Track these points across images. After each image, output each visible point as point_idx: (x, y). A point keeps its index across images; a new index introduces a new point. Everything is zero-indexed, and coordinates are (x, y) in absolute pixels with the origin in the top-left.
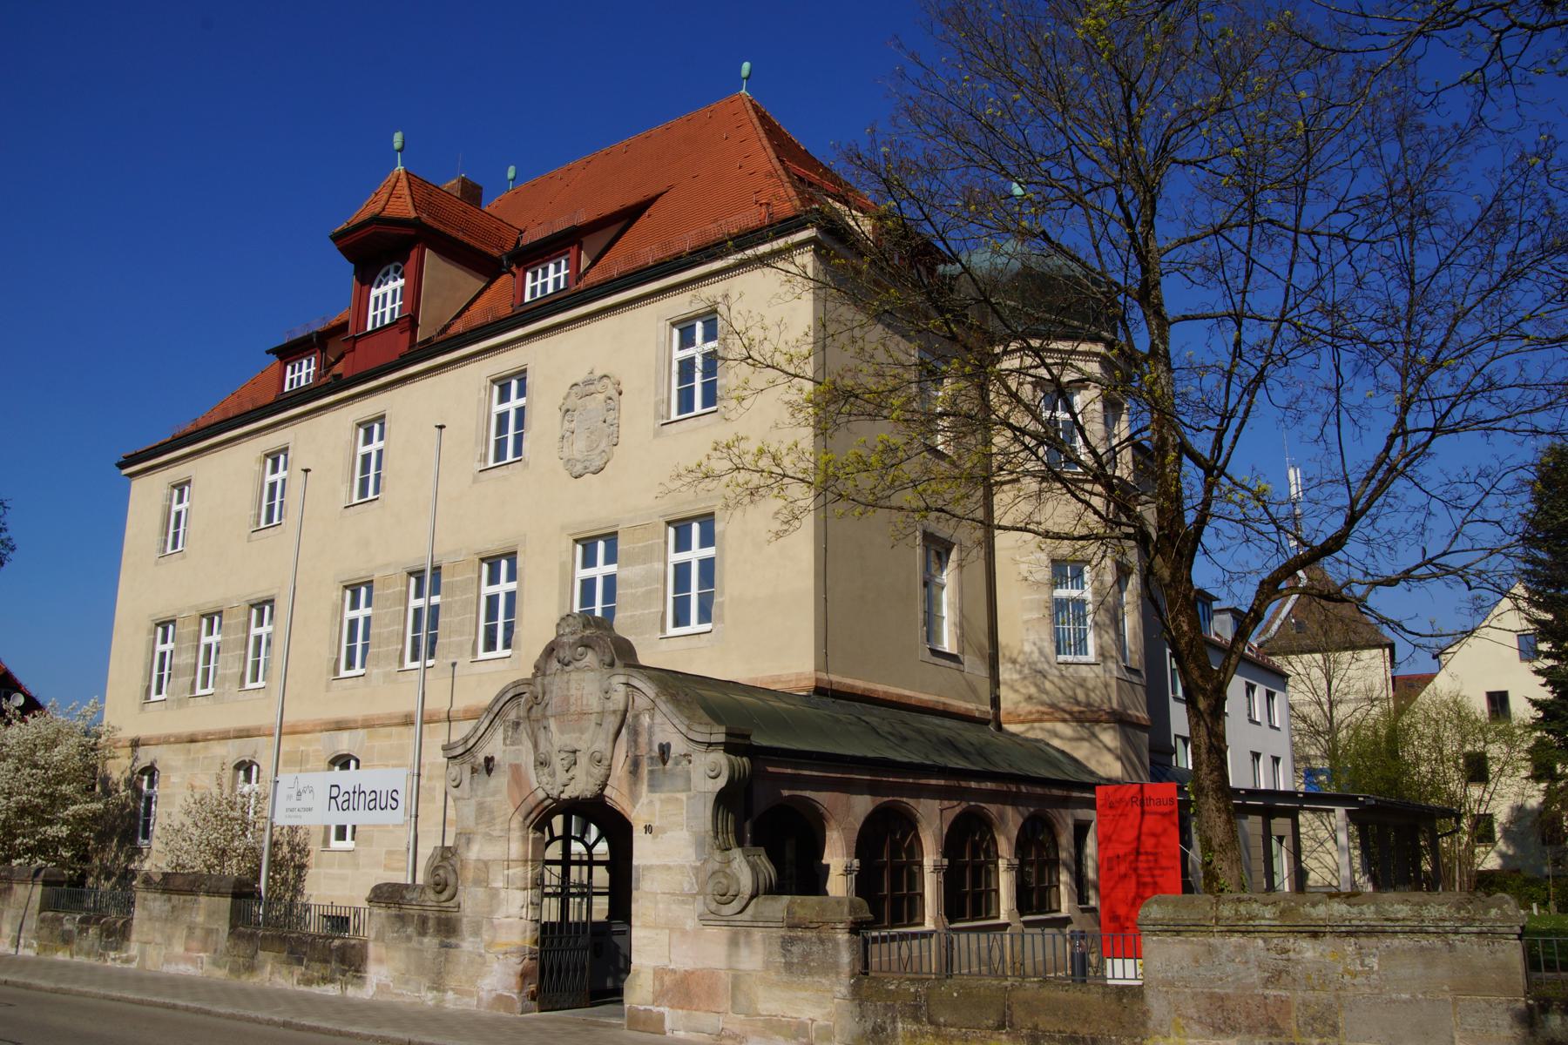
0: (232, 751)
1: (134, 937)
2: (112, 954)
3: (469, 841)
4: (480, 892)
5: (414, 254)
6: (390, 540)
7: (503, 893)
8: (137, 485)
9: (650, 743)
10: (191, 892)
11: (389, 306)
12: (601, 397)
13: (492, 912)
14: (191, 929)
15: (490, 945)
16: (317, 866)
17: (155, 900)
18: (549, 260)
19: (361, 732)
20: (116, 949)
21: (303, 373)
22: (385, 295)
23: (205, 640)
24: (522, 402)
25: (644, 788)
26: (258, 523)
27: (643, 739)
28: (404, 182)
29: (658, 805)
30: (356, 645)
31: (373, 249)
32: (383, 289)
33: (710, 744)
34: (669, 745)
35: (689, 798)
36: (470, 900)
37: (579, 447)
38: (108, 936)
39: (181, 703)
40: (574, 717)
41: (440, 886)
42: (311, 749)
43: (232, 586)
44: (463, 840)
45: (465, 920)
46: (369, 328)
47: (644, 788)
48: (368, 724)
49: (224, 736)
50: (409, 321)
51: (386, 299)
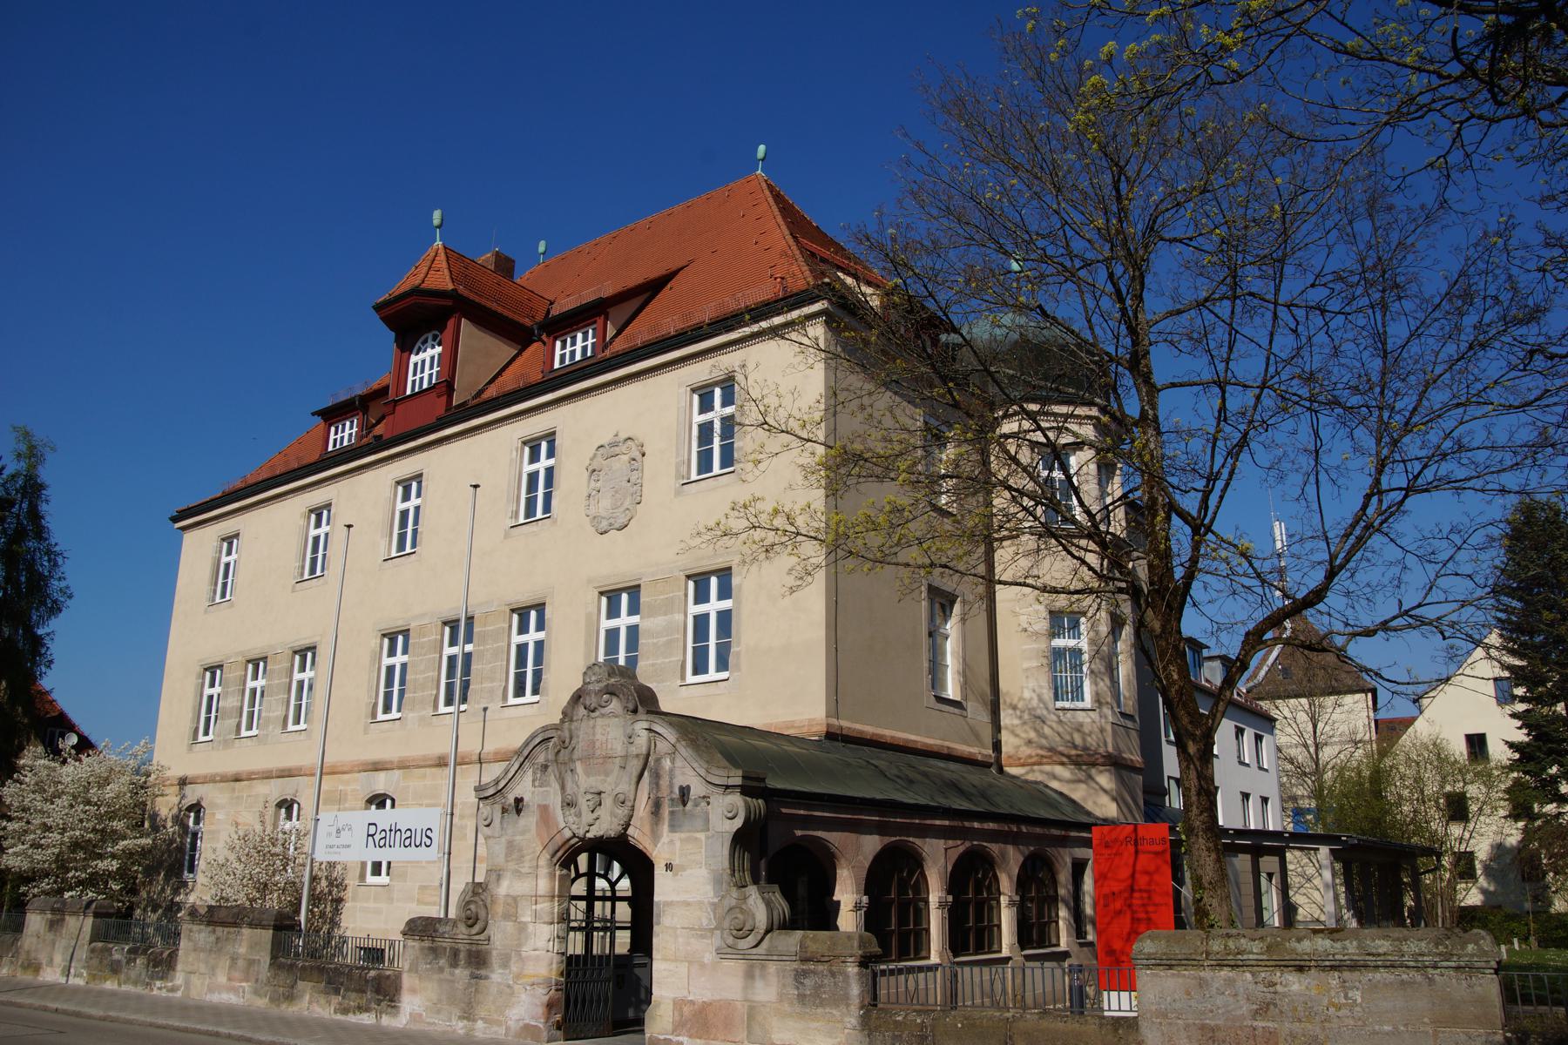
0: (275, 790)
1: (179, 967)
2: (158, 983)
3: (499, 878)
4: (509, 926)
5: (451, 324)
6: (425, 591)
7: (531, 927)
8: (189, 537)
9: (671, 785)
10: (235, 924)
11: (427, 371)
12: (626, 458)
13: (520, 945)
14: (234, 959)
15: (518, 976)
16: (354, 899)
17: (200, 931)
18: (578, 330)
19: (397, 772)
20: (162, 979)
21: (346, 433)
22: (423, 362)
23: (250, 684)
24: (551, 462)
25: (665, 827)
26: (302, 574)
27: (664, 782)
28: (442, 256)
29: (678, 844)
30: (393, 691)
31: (413, 318)
32: (422, 356)
33: (727, 787)
34: (688, 787)
35: (707, 838)
36: (500, 934)
37: (604, 505)
38: (155, 966)
39: (226, 744)
40: (599, 761)
41: (471, 920)
42: (349, 788)
43: (277, 637)
44: (494, 877)
45: (494, 953)
46: (409, 392)
47: (665, 827)
48: (404, 765)
49: (267, 776)
50: (445, 386)
51: (425, 364)
